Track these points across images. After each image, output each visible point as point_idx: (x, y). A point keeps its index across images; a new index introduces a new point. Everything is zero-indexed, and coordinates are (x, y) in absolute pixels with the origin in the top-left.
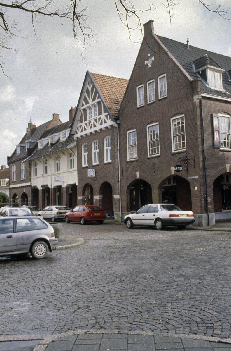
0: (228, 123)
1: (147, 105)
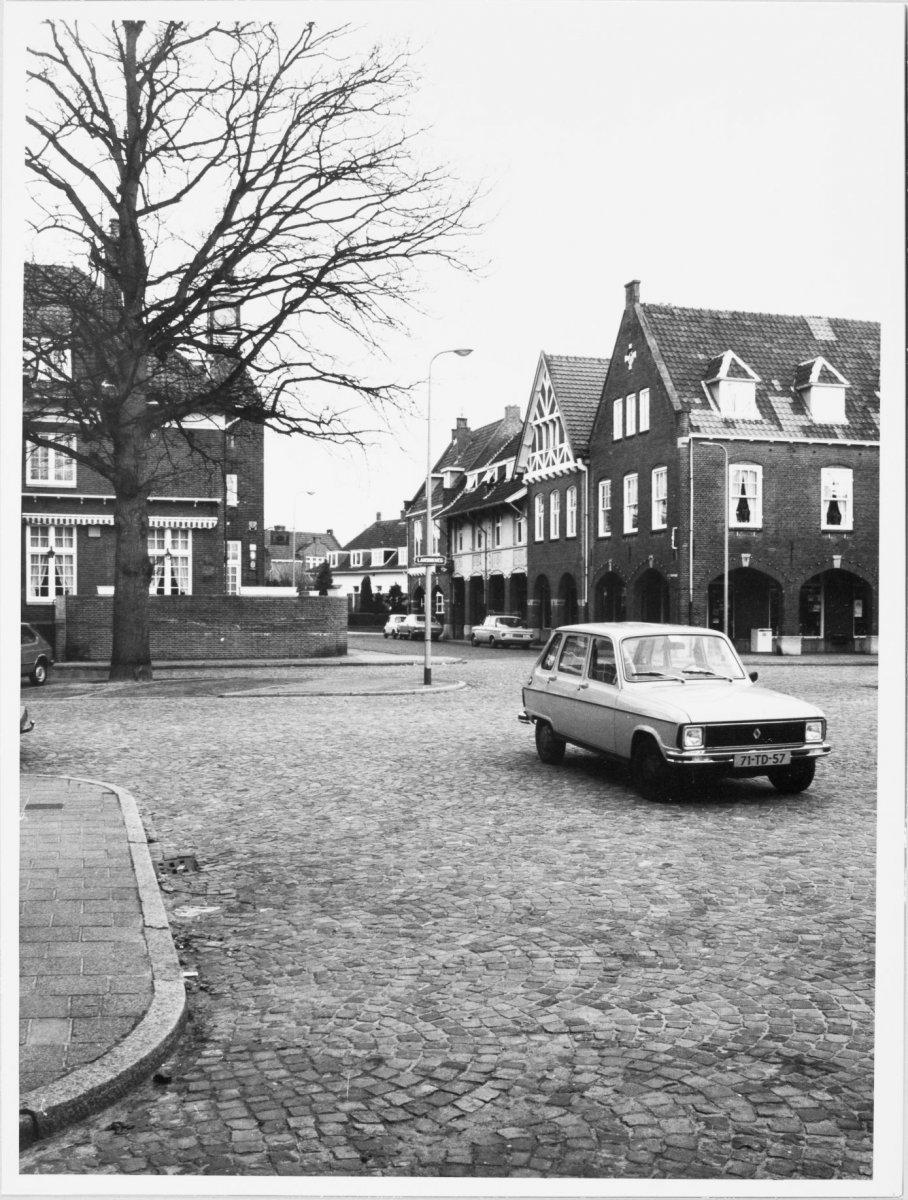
1: (626, 438)
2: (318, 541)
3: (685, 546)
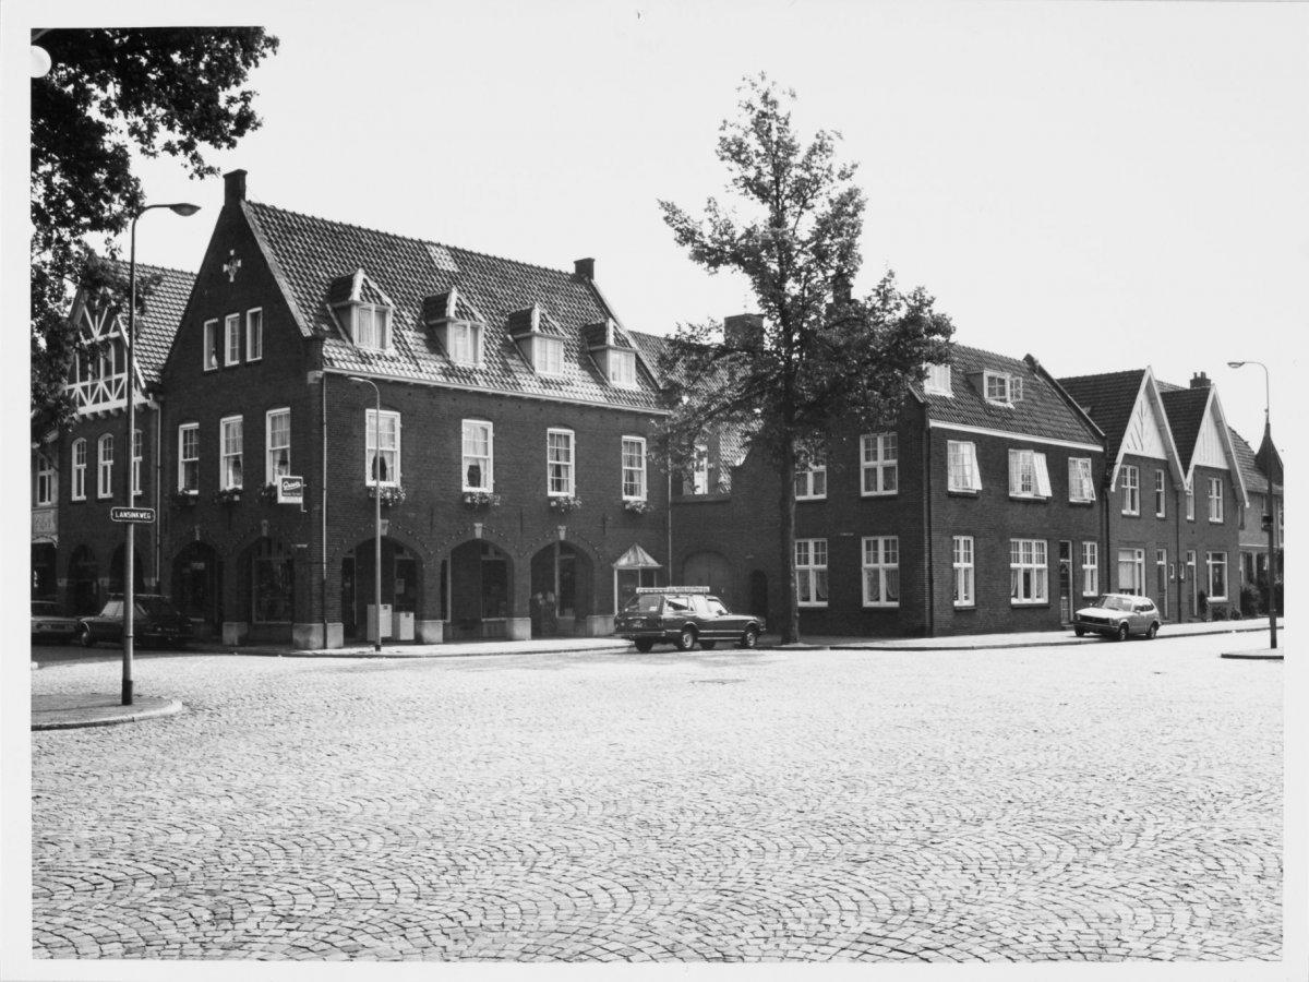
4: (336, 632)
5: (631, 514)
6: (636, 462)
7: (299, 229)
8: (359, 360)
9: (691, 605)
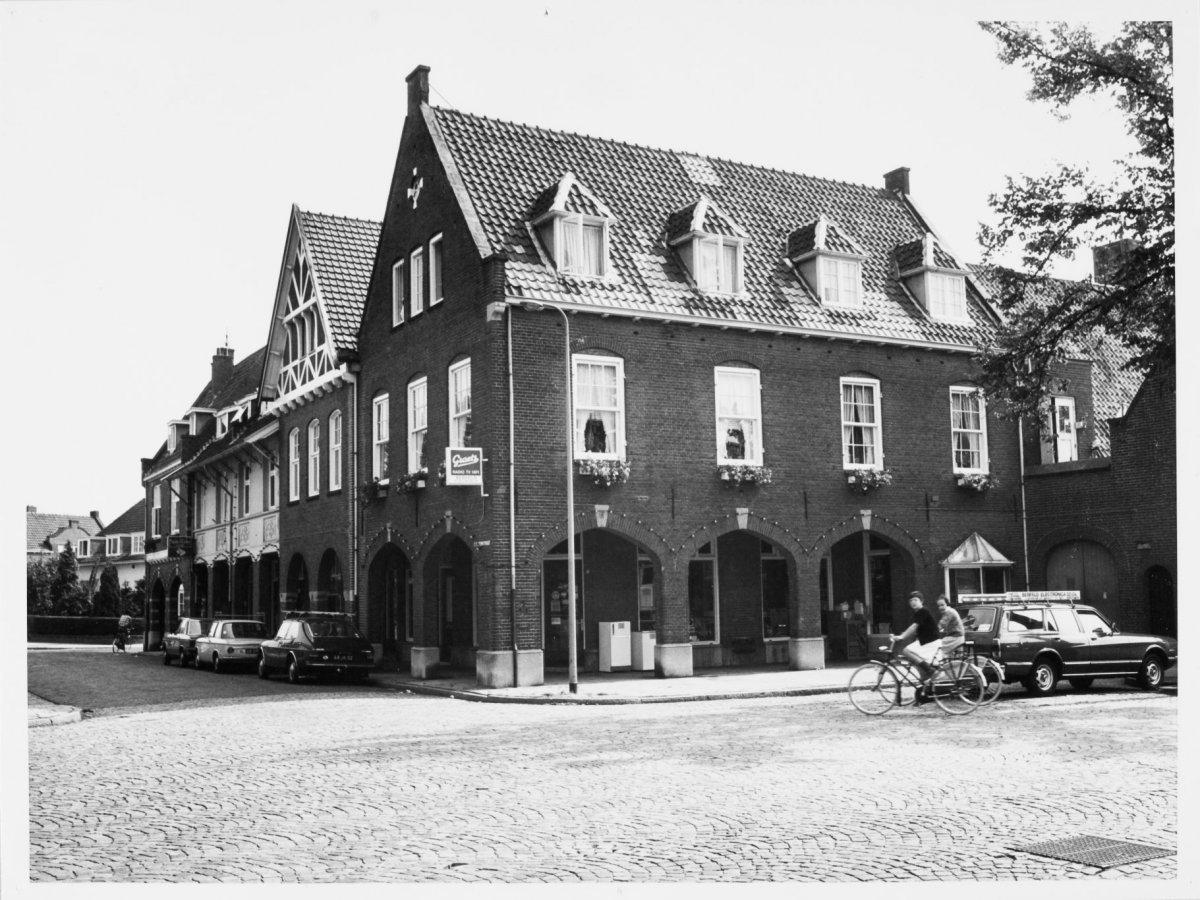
0: (133, 567)
2: (74, 525)
3: (501, 490)
4: (532, 662)
5: (968, 493)
6: (972, 422)
7: (502, 138)
8: (562, 288)
9: (1048, 619)
